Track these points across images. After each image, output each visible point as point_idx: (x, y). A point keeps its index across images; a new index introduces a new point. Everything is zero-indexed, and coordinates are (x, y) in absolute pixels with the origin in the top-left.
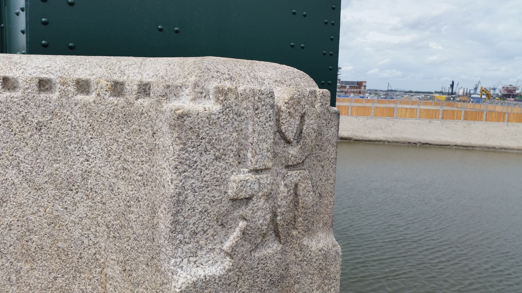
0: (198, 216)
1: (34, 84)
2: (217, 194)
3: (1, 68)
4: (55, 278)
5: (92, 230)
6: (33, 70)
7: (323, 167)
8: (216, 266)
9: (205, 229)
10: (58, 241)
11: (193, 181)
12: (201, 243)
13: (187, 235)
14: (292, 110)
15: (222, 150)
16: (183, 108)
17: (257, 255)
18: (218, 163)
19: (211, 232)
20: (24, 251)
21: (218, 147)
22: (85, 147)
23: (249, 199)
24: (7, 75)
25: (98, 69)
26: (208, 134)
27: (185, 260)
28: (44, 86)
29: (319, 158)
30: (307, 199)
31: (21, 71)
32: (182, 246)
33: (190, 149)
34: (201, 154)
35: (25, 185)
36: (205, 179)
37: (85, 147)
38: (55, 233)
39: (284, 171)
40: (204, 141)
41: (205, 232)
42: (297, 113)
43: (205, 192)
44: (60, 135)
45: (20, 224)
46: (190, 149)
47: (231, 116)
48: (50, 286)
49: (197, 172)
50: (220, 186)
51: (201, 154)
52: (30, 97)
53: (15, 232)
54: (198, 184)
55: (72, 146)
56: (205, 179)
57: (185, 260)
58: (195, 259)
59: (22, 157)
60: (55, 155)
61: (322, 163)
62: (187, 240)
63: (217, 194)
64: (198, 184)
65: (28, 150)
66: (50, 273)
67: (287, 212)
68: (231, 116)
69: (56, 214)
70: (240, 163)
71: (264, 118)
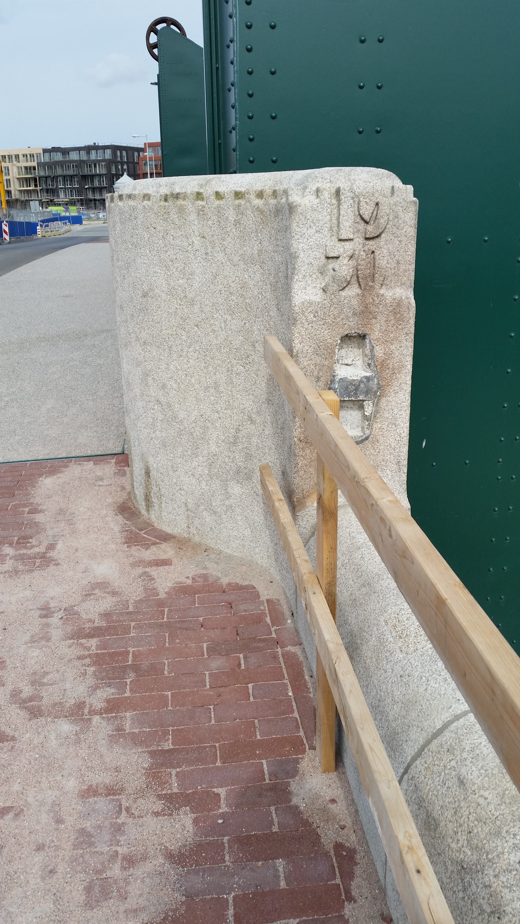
0: (306, 266)
1: (232, 195)
2: (317, 254)
3: (519, 885)
4: (245, 324)
5: (264, 289)
6: (233, 186)
7: (400, 241)
8: (317, 296)
9: (311, 274)
10: (246, 298)
11: (303, 245)
12: (308, 282)
13: (301, 277)
14: (368, 200)
15: (320, 227)
16: (297, 201)
17: (343, 294)
18: (318, 235)
19: (314, 276)
20: (228, 308)
21: (318, 225)
22: (259, 234)
23: (337, 258)
24: (218, 190)
25: (269, 181)
26: (311, 217)
27: (300, 291)
28: (238, 196)
29: (396, 235)
30: (382, 262)
31: (225, 187)
32: (298, 283)
33: (301, 226)
34: (308, 229)
35: (228, 263)
36: (310, 244)
37: (259, 234)
38: (244, 293)
39: (365, 241)
40: (309, 221)
41: (311, 276)
42: (371, 202)
43: (310, 252)
44: (246, 228)
45: (226, 289)
46: (301, 226)
47: (326, 205)
48: (242, 329)
49: (306, 240)
50: (319, 249)
51: (308, 229)
52: (230, 204)
53: (223, 295)
54: (306, 247)
55: (253, 234)
56: (310, 244)
57: (300, 291)
58: (305, 291)
59: (226, 244)
60: (244, 241)
61: (399, 239)
62: (301, 280)
63: (317, 254)
64: (306, 247)
65: (229, 239)
66: (242, 321)
67: (365, 269)
68: (326, 205)
69: (245, 281)
70: (373, 252)
71: (346, 206)
